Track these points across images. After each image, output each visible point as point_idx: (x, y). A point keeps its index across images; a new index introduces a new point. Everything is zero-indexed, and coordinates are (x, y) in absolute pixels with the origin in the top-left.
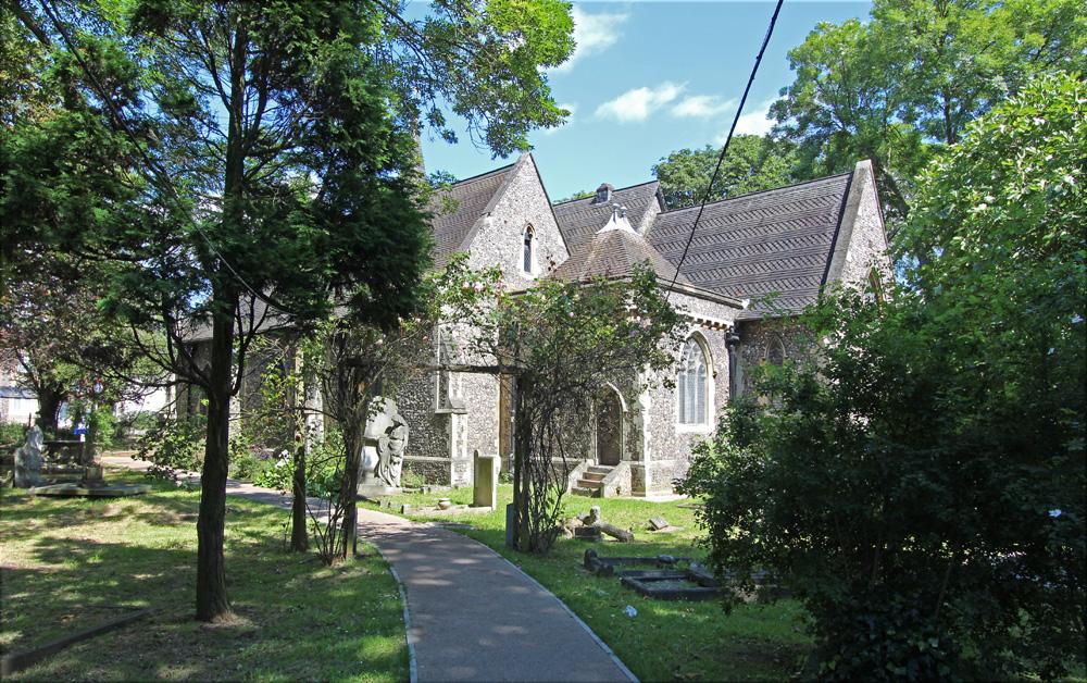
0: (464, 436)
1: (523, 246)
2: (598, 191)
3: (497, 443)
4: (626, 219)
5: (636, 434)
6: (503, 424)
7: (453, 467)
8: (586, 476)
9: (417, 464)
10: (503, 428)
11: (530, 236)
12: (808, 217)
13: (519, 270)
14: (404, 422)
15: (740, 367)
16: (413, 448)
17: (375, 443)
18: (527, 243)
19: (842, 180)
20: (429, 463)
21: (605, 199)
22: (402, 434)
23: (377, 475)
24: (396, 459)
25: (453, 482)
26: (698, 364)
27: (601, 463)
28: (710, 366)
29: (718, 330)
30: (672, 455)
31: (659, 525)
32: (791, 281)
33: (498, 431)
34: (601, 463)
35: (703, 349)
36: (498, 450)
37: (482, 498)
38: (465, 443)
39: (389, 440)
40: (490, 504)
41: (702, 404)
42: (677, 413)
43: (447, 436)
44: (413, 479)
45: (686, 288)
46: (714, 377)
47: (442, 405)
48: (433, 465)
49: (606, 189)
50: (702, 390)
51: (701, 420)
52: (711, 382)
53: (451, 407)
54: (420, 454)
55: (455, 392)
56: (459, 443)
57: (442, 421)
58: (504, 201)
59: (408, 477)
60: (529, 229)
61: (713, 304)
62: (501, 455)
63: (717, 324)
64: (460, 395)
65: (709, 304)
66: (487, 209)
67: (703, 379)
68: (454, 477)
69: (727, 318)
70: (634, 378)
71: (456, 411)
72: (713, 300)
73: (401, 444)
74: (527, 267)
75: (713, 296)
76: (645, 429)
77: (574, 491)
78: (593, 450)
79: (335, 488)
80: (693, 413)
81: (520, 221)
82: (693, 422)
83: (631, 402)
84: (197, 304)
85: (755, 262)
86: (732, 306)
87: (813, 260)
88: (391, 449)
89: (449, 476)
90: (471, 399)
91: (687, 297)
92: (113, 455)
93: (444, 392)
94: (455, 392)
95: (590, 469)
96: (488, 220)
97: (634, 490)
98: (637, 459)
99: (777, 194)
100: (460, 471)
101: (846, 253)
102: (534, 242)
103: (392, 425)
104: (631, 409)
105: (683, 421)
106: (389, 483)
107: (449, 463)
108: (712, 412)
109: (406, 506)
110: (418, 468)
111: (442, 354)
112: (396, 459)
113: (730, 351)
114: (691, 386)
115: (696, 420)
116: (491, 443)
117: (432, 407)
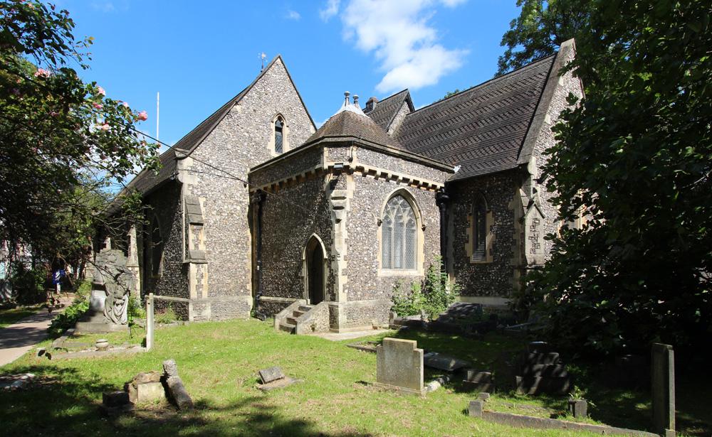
0: (204, 282)
2: (367, 104)
5: (333, 278)
10: (255, 276)
12: (516, 94)
13: (269, 150)
15: (451, 222)
18: (279, 129)
19: (548, 61)
26: (406, 219)
28: (419, 220)
29: (419, 187)
30: (373, 295)
31: (268, 378)
32: (496, 146)
35: (411, 205)
36: (251, 292)
42: (379, 259)
45: (389, 150)
46: (424, 229)
50: (411, 241)
51: (410, 265)
52: (420, 235)
55: (196, 246)
56: (199, 287)
60: (280, 119)
61: (422, 166)
62: (253, 296)
63: (425, 185)
64: (202, 247)
65: (416, 166)
67: (413, 231)
68: (192, 315)
69: (438, 180)
70: (331, 228)
72: (421, 163)
75: (422, 159)
77: (282, 327)
78: (306, 293)
80: (401, 260)
81: (270, 112)
82: (401, 267)
83: (328, 250)
85: (468, 137)
86: (442, 170)
89: (187, 312)
90: (221, 252)
91: (391, 158)
94: (196, 246)
97: (331, 327)
99: (494, 83)
100: (199, 309)
101: (544, 116)
102: (286, 130)
104: (330, 256)
105: (384, 267)
107: (188, 303)
113: (441, 209)
114: (398, 236)
115: (404, 265)
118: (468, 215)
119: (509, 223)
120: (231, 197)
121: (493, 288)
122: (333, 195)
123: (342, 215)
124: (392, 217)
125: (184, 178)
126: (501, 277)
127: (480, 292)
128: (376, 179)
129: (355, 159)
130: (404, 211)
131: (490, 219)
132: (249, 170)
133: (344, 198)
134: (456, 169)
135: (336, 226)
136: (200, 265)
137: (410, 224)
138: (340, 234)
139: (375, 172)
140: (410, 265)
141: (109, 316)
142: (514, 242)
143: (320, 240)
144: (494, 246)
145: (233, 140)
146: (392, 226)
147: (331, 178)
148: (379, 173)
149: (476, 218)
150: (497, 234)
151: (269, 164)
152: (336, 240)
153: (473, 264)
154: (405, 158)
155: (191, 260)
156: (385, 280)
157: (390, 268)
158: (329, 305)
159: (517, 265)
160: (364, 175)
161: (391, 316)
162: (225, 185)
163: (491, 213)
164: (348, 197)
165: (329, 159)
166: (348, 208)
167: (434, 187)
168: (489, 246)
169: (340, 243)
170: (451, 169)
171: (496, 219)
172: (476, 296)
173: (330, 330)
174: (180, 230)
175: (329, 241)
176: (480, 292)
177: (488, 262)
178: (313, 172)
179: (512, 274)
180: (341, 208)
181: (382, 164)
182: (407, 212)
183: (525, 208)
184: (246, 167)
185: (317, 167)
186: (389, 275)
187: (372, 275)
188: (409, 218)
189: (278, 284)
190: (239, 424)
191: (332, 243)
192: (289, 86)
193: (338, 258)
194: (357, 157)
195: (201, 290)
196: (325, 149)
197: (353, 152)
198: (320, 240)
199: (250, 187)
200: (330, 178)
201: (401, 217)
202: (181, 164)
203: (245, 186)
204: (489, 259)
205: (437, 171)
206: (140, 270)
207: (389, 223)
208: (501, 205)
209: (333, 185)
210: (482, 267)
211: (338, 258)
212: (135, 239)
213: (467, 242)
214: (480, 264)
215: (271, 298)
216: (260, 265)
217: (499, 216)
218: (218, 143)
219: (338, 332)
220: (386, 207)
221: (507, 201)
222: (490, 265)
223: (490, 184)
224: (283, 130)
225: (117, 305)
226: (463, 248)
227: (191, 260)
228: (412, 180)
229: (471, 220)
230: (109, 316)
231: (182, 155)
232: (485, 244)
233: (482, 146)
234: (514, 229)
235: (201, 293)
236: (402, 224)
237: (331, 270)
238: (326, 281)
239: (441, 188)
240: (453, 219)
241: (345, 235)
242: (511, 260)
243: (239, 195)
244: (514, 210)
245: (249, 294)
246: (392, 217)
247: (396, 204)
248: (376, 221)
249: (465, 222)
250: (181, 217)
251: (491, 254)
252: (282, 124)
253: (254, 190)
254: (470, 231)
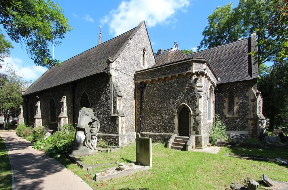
1: (142, 57)
2: (158, 51)
3: (134, 128)
6: (137, 121)
7: (120, 138)
8: (175, 140)
9: (104, 137)
11: (144, 53)
14: (97, 120)
16: (102, 130)
17: (83, 130)
18: (143, 55)
20: (109, 136)
21: (160, 53)
22: (97, 125)
23: (84, 145)
24: (94, 137)
25: (120, 144)
27: (179, 135)
33: (135, 123)
34: (179, 135)
36: (135, 130)
37: (142, 160)
38: (124, 128)
39: (90, 128)
40: (149, 165)
43: (117, 125)
44: (103, 143)
47: (114, 113)
48: (111, 137)
49: (161, 50)
53: (118, 113)
54: (106, 133)
55: (119, 107)
56: (122, 128)
57: (114, 120)
59: (100, 142)
64: (121, 108)
66: (130, 37)
68: (120, 143)
71: (120, 115)
73: (96, 130)
76: (202, 121)
77: (172, 148)
79: (62, 153)
81: (141, 47)
83: (194, 111)
87: (242, 64)
88: (91, 132)
89: (118, 142)
92: (8, 132)
93: (115, 107)
94: (119, 107)
95: (176, 138)
98: (198, 134)
100: (123, 140)
103: (92, 121)
106: (91, 149)
107: (118, 137)
109: (98, 174)
110: (105, 138)
111: (113, 92)
112: (94, 137)
116: (133, 128)
117: (110, 114)
118: (225, 98)
119: (246, 102)
121: (237, 127)
122: (197, 85)
125: (112, 72)
126: (242, 122)
127: (230, 129)
131: (236, 100)
133: (202, 87)
136: (123, 117)
141: (88, 145)
142: (44, 111)
143: (188, 106)
144: (238, 111)
145: (130, 57)
147: (195, 78)
149: (229, 99)
150: (240, 106)
151: (152, 69)
152: (199, 106)
153: (227, 118)
155: (119, 115)
158: (195, 136)
159: (250, 118)
162: (127, 78)
163: (237, 97)
165: (195, 68)
168: (236, 110)
171: (240, 100)
172: (229, 131)
173: (196, 148)
174: (108, 99)
175: (195, 107)
176: (230, 129)
177: (235, 117)
179: (247, 122)
180: (201, 91)
183: (256, 96)
185: (188, 72)
189: (155, 127)
190: (46, 172)
191: (197, 107)
192: (147, 36)
193: (201, 115)
195: (123, 129)
196: (194, 63)
198: (188, 106)
199: (135, 81)
200: (194, 77)
202: (111, 65)
204: (236, 116)
206: (68, 119)
208: (242, 94)
209: (196, 80)
210: (232, 120)
211: (201, 115)
212: (66, 104)
213: (225, 109)
214: (231, 118)
215: (150, 133)
216: (142, 117)
217: (241, 99)
219: (202, 149)
221: (245, 93)
222: (236, 118)
223: (236, 85)
225: (93, 139)
226: (222, 111)
227: (119, 115)
229: (227, 100)
230: (88, 145)
232: (234, 109)
233: (227, 70)
234: (248, 104)
235: (123, 132)
237: (195, 120)
238: (192, 125)
240: (217, 99)
242: (247, 116)
243: (131, 84)
244: (248, 96)
245: (134, 131)
249: (224, 101)
250: (110, 92)
251: (237, 114)
253: (139, 82)
254: (226, 105)
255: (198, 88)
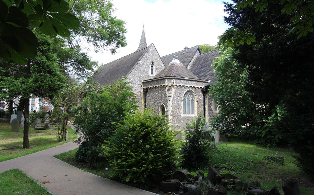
4: (178, 59)
13: (149, 74)
18: (152, 66)
26: (191, 99)
30: (180, 122)
41: (193, 109)
42: (182, 111)
45: (185, 79)
46: (197, 101)
51: (193, 113)
52: (196, 103)
58: (145, 57)
60: (152, 63)
61: (196, 82)
65: (194, 82)
66: (139, 59)
67: (194, 102)
74: (152, 73)
81: (150, 61)
83: (167, 109)
84: (30, 100)
86: (204, 82)
91: (185, 81)
92: (60, 145)
96: (140, 62)
102: (154, 67)
105: (183, 114)
108: (196, 110)
114: (188, 104)
120: (137, 90)
123: (171, 99)
124: (186, 98)
128: (181, 88)
129: (174, 83)
130: (190, 96)
132: (143, 81)
134: (209, 81)
135: (169, 102)
137: (193, 100)
138: (170, 104)
139: (181, 86)
140: (193, 113)
146: (186, 101)
148: (182, 86)
152: (169, 106)
154: (190, 80)
156: (184, 118)
157: (186, 114)
160: (177, 87)
161: (185, 129)
162: (135, 87)
164: (172, 94)
166: (172, 97)
167: (201, 88)
169: (170, 107)
170: (207, 81)
175: (167, 107)
178: (160, 86)
180: (170, 97)
181: (182, 83)
182: (191, 97)
184: (142, 80)
186: (185, 116)
187: (180, 116)
188: (192, 98)
191: (168, 107)
192: (156, 52)
194: (175, 82)
197: (174, 81)
201: (189, 98)
203: (141, 86)
205: (202, 83)
207: (185, 100)
218: (134, 73)
220: (184, 95)
224: (154, 67)
228: (193, 87)
231: (124, 78)
236: (190, 100)
239: (203, 88)
241: (171, 104)
246: (186, 98)
247: (188, 94)
248: (181, 100)
252: (153, 65)
255: (168, 95)
